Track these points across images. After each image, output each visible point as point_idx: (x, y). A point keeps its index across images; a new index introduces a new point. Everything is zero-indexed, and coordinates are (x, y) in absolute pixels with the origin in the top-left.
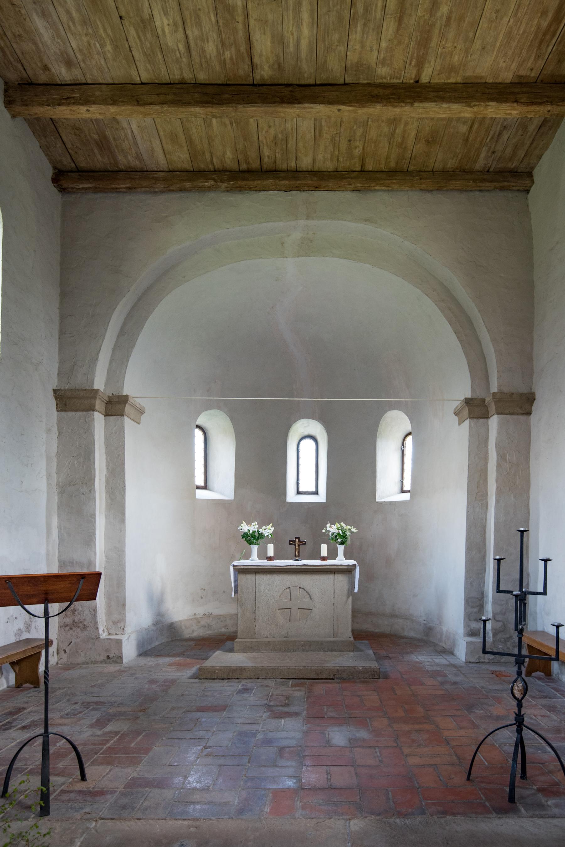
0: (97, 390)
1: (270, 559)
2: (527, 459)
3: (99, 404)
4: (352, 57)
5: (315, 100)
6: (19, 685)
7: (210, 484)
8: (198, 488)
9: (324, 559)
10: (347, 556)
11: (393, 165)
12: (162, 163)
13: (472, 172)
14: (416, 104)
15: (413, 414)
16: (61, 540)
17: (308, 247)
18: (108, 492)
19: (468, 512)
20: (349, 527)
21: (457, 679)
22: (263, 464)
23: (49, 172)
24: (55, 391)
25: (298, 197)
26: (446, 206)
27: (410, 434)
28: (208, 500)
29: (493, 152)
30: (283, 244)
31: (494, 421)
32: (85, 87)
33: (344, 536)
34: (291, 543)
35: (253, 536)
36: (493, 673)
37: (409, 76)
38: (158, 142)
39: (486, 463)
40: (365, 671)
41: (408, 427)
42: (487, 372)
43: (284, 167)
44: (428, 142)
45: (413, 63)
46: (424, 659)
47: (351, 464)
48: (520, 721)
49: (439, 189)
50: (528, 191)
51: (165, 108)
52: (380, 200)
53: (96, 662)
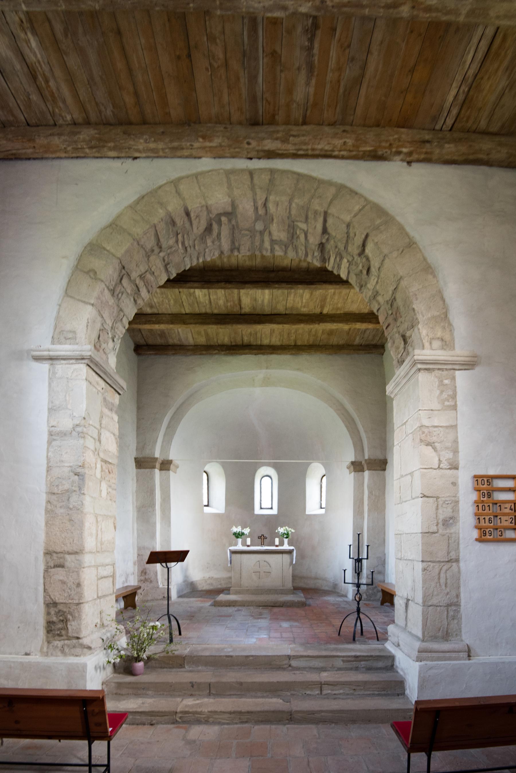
0: (157, 458)
1: (248, 546)
2: (384, 493)
3: (158, 465)
4: (289, 305)
5: (271, 322)
6: (126, 607)
7: (210, 504)
8: (205, 506)
9: (277, 546)
10: (289, 544)
11: (311, 343)
12: (191, 341)
13: (353, 346)
14: (321, 324)
15: (326, 466)
16: (138, 536)
17: (267, 382)
18: (161, 511)
19: (354, 521)
20: (290, 529)
21: (346, 606)
22: (241, 492)
23: (132, 346)
24: (135, 459)
25: (262, 358)
26: (339, 362)
27: (324, 475)
28: (210, 513)
29: (363, 338)
30: (254, 380)
31: (367, 473)
32: (158, 316)
33: (288, 534)
34: (260, 537)
35: (239, 534)
36: (365, 604)
37: (318, 311)
38: (190, 334)
39: (363, 495)
40: (299, 602)
41: (323, 472)
42: (363, 447)
43: (255, 344)
44: (328, 334)
45: (319, 307)
46: (331, 599)
47: (291, 491)
48: (358, 611)
49: (336, 353)
50: (383, 354)
51: (197, 325)
52: (304, 359)
53: (157, 600)
